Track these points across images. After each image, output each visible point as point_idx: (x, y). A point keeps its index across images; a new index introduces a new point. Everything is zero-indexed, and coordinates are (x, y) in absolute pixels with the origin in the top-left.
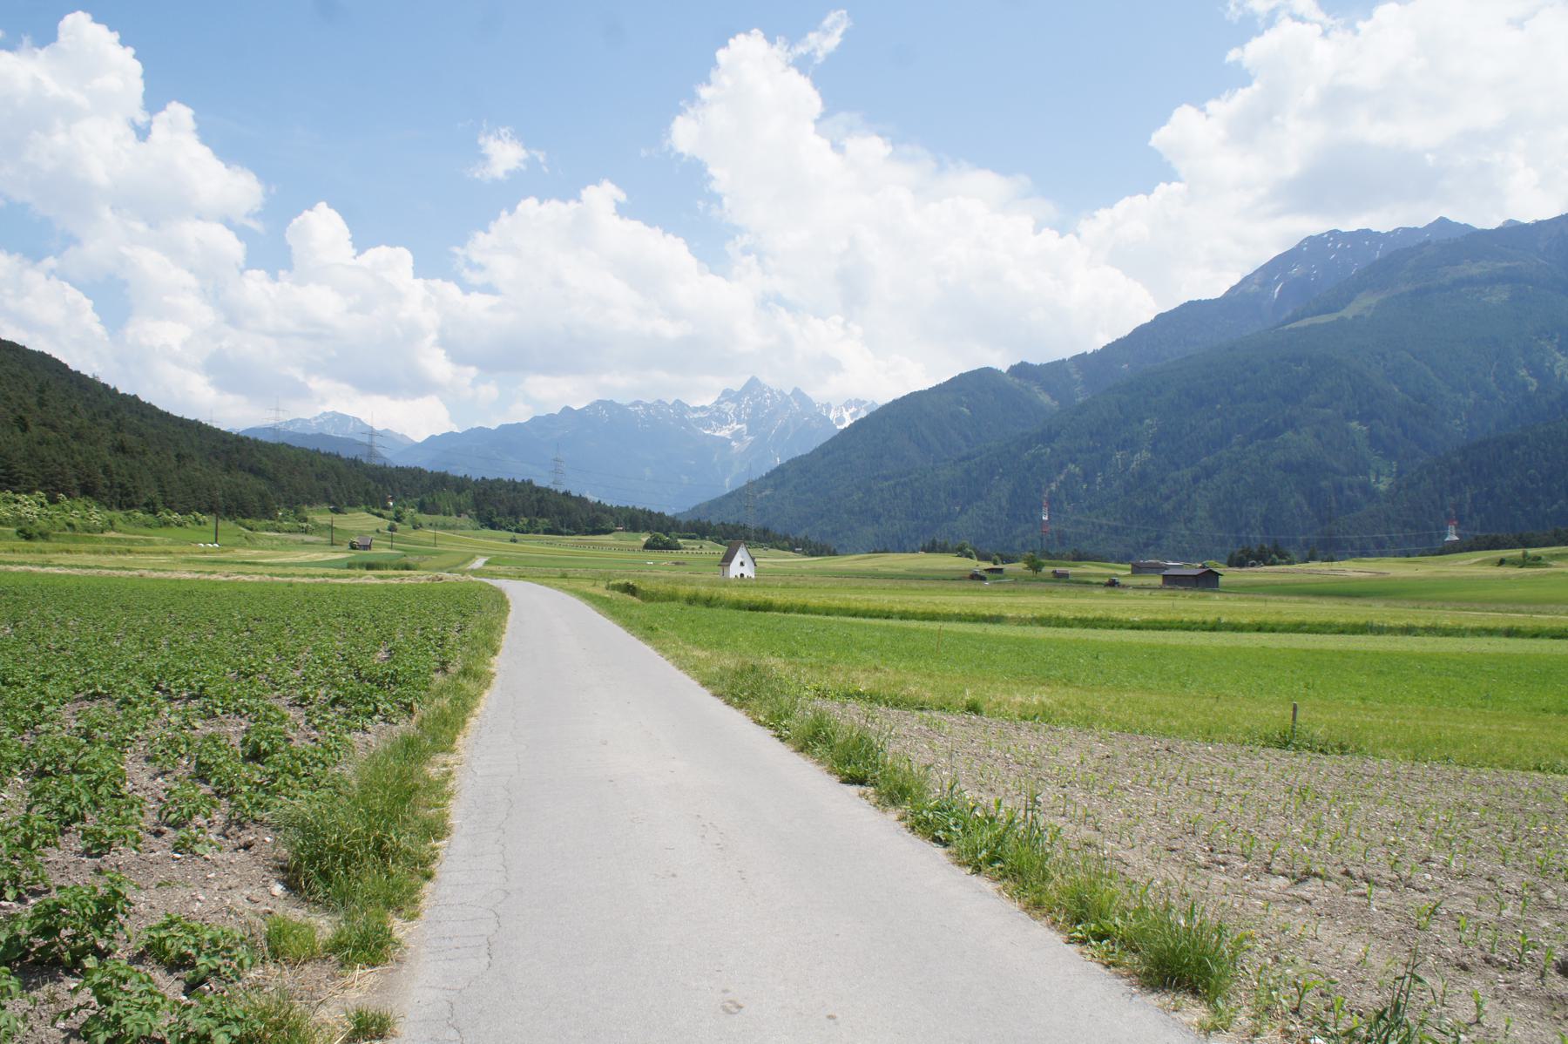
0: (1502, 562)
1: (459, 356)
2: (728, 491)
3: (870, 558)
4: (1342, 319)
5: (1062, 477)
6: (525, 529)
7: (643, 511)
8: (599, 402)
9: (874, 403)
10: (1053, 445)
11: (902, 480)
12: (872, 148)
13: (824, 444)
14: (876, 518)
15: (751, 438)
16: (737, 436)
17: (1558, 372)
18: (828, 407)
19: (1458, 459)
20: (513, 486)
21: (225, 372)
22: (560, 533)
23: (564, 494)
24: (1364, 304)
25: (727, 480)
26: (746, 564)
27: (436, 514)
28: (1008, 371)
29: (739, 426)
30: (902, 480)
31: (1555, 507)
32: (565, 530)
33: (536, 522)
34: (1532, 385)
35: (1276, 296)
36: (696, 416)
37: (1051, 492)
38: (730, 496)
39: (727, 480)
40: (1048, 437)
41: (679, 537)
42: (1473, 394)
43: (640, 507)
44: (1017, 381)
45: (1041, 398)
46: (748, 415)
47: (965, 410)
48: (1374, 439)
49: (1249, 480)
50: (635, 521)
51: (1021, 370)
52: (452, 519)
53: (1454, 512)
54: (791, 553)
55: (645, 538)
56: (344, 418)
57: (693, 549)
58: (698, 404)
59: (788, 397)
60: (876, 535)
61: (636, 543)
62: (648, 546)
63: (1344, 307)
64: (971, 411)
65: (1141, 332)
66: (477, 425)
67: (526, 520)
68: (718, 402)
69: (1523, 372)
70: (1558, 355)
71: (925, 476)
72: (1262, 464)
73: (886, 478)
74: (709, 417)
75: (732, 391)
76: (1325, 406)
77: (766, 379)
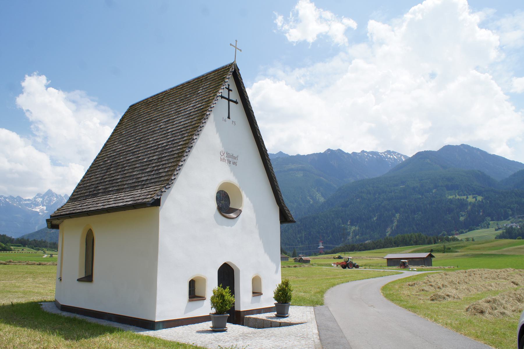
16: (42, 211)
17: (317, 198)
29: (43, 207)
34: (311, 201)
36: (26, 202)
39: (37, 227)
41: (12, 246)
46: (47, 203)
53: (300, 240)
57: (18, 251)
58: (27, 198)
59: (63, 197)
68: (35, 198)
69: (308, 198)
70: (317, 193)
74: (31, 203)
75: (41, 194)
77: (55, 190)
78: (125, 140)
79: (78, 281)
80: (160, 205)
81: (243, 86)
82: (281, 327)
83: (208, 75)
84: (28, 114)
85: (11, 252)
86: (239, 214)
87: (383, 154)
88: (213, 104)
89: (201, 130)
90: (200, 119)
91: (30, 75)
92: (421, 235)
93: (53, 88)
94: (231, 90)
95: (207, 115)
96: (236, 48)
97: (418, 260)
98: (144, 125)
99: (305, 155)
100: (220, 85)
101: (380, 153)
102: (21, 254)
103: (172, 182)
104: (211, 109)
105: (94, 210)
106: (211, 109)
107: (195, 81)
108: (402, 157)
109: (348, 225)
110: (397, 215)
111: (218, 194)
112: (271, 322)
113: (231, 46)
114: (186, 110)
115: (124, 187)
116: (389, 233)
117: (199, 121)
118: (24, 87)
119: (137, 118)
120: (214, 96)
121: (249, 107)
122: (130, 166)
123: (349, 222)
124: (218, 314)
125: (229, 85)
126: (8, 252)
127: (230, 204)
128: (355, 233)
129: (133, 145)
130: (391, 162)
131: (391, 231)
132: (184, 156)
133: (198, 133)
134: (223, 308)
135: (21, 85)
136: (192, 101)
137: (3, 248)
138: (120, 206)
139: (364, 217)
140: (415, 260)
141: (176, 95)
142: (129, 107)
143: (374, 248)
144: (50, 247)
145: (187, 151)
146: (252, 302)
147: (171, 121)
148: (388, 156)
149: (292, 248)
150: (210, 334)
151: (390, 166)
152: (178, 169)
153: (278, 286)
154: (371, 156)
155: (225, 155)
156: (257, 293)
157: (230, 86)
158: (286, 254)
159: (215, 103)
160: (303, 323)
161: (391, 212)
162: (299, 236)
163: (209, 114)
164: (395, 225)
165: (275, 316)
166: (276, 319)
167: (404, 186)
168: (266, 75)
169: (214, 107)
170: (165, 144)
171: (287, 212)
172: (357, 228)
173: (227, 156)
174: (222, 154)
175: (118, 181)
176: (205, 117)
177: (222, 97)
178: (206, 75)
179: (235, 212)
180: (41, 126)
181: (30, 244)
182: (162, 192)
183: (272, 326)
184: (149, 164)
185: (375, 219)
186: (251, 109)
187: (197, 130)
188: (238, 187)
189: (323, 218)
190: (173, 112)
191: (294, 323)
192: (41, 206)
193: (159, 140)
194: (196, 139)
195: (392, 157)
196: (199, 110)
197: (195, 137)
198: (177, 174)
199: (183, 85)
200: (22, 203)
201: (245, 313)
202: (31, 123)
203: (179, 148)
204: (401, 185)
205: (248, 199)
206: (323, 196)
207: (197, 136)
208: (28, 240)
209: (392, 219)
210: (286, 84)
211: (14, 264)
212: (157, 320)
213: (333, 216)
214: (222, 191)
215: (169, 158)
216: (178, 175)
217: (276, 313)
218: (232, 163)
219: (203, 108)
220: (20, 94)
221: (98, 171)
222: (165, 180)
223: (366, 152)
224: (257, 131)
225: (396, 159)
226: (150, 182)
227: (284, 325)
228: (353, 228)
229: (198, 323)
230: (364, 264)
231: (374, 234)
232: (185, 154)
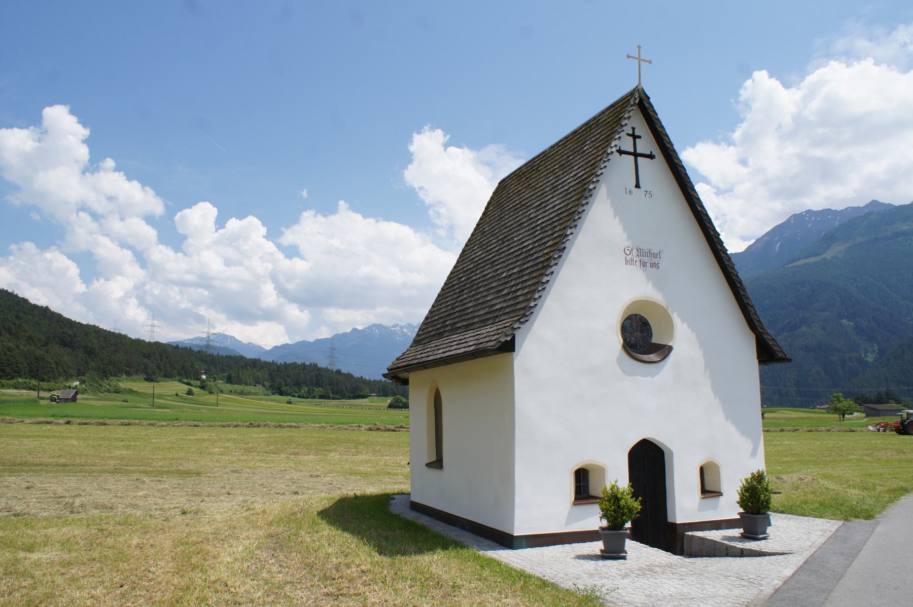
4: (825, 259)
6: (305, 394)
8: (374, 325)
21: (157, 311)
22: (329, 398)
23: (336, 371)
24: (834, 252)
27: (240, 384)
33: (314, 390)
35: (777, 249)
52: (251, 388)
55: (389, 400)
56: (225, 337)
62: (391, 406)
67: (306, 389)
78: (486, 241)
79: (426, 467)
80: (514, 351)
81: (659, 124)
82: (744, 557)
83: (600, 115)
84: (421, 195)
86: (667, 354)
88: (601, 169)
89: (580, 218)
90: (579, 199)
91: (419, 133)
93: (454, 146)
94: (639, 137)
95: (590, 190)
96: (639, 60)
98: (511, 214)
100: (613, 132)
103: (531, 311)
104: (597, 179)
105: (431, 360)
106: (597, 179)
107: (582, 129)
111: (629, 321)
112: (727, 547)
113: (630, 58)
114: (564, 184)
115: (474, 321)
117: (577, 202)
118: (413, 152)
119: (505, 202)
120: (602, 154)
121: (676, 161)
122: (486, 285)
124: (612, 530)
125: (633, 129)
127: (652, 337)
129: (492, 251)
132: (551, 266)
133: (575, 223)
134: (617, 520)
135: (409, 151)
136: (574, 166)
137: (404, 404)
138: (461, 353)
141: (556, 158)
142: (498, 184)
145: (556, 256)
146: (700, 509)
147: (544, 205)
150: (593, 562)
152: (540, 289)
153: (744, 483)
155: (635, 252)
156: (709, 491)
157: (636, 130)
158: (899, 403)
159: (605, 167)
160: (786, 554)
163: (595, 188)
165: (740, 535)
166: (737, 543)
168: (829, 56)
169: (602, 173)
170: (530, 247)
171: (770, 343)
173: (639, 255)
174: (628, 252)
175: (470, 311)
176: (587, 194)
177: (621, 152)
178: (598, 117)
179: (661, 351)
180: (442, 211)
182: (514, 329)
183: (729, 554)
184: (508, 282)
186: (680, 163)
187: (572, 219)
188: (663, 307)
190: (548, 189)
191: (767, 552)
193: (524, 240)
194: (572, 233)
196: (580, 181)
197: (569, 232)
198: (540, 297)
199: (566, 138)
201: (686, 527)
202: (430, 206)
203: (545, 252)
205: (685, 325)
207: (574, 229)
210: (875, 64)
211: (406, 431)
212: (517, 533)
214: (636, 315)
215: (532, 269)
216: (541, 299)
217: (741, 530)
218: (648, 264)
219: (585, 179)
220: (409, 164)
221: (450, 294)
222: (521, 308)
224: (696, 202)
226: (504, 312)
227: (748, 553)
229: (592, 541)
232: (553, 262)
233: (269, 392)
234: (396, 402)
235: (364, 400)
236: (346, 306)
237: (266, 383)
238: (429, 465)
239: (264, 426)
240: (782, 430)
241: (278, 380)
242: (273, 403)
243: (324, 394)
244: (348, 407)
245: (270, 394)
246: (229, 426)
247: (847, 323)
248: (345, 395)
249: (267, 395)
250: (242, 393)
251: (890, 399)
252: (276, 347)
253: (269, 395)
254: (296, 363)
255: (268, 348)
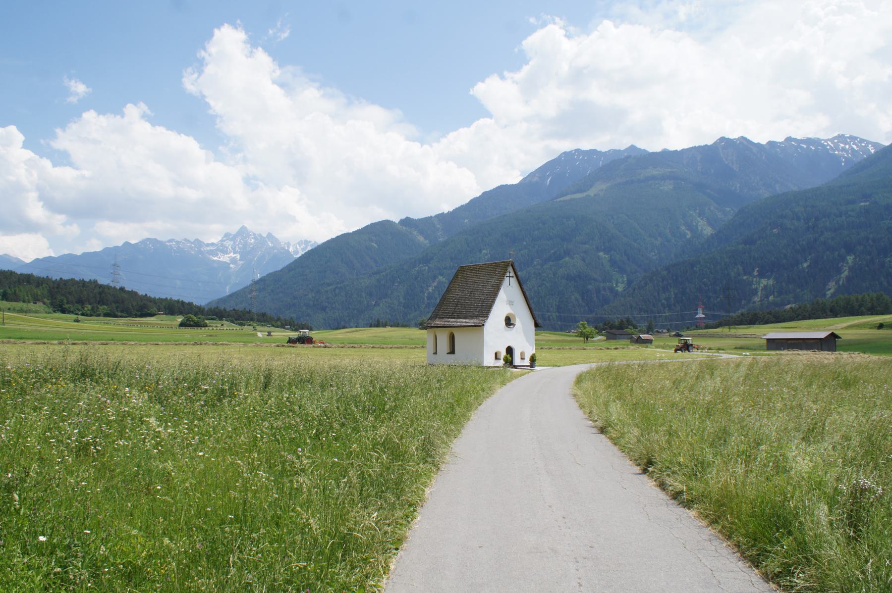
0: (881, 326)
1: (52, 206)
2: (228, 294)
3: (357, 331)
5: (435, 284)
6: (89, 312)
7: (178, 301)
8: (148, 239)
9: (315, 242)
10: (430, 265)
11: (339, 286)
12: (311, 94)
13: (289, 264)
14: (324, 309)
15: (241, 262)
16: (234, 261)
17: (700, 228)
18: (289, 244)
19: (665, 273)
20: (83, 283)
22: (116, 316)
24: (598, 188)
25: (228, 287)
26: (518, 322)
28: (399, 222)
29: (235, 255)
30: (339, 286)
31: (719, 299)
32: (119, 314)
33: (98, 308)
36: (208, 248)
37: (429, 293)
38: (231, 296)
39: (228, 287)
40: (426, 260)
41: (207, 319)
42: (659, 239)
43: (175, 298)
44: (404, 228)
45: (419, 238)
46: (240, 248)
47: (375, 245)
48: (613, 263)
49: (548, 285)
50: (171, 308)
51: (407, 222)
52: (31, 306)
53: (666, 303)
54: (282, 329)
55: (180, 319)
57: (217, 326)
59: (264, 238)
60: (325, 320)
61: (173, 323)
62: (182, 325)
63: (589, 190)
64: (378, 245)
65: (474, 202)
66: (66, 252)
67: (90, 307)
69: (683, 228)
70: (699, 219)
71: (353, 283)
72: (554, 275)
73: (329, 285)
75: (230, 234)
76: (585, 243)
77: (249, 225)
85: (207, 328)
87: (830, 143)
92: (882, 296)
97: (812, 341)
99: (676, 150)
101: (823, 140)
102: (228, 331)
108: (870, 146)
109: (755, 277)
110: (850, 259)
116: (832, 291)
123: (756, 271)
126: (203, 328)
128: (767, 291)
130: (845, 157)
131: (835, 287)
137: (195, 323)
139: (784, 261)
140: (808, 341)
143: (791, 319)
144: (257, 321)
148: (840, 145)
149: (651, 316)
151: (843, 164)
154: (805, 146)
156: (522, 358)
161: (837, 253)
162: (664, 296)
164: (844, 276)
167: (868, 203)
172: (771, 282)
181: (229, 316)
185: (805, 265)
189: (708, 265)
192: (232, 254)
195: (847, 147)
200: (202, 249)
204: (862, 202)
206: (710, 224)
208: (225, 310)
209: (840, 265)
213: (727, 260)
223: (795, 140)
225: (856, 151)
228: (764, 282)
230: (740, 346)
231: (803, 292)
233: (51, 310)
234: (187, 320)
235: (152, 318)
236: (114, 218)
237: (45, 300)
238: (434, 354)
239: (205, 344)
240: (542, 348)
241: (59, 297)
242: (60, 322)
243: (108, 312)
244: (139, 326)
245: (52, 312)
246: (180, 344)
247: (604, 256)
248: (131, 313)
249: (48, 313)
250: (21, 311)
251: (629, 325)
252: (37, 260)
253: (51, 313)
254: (74, 279)
255: (28, 261)
